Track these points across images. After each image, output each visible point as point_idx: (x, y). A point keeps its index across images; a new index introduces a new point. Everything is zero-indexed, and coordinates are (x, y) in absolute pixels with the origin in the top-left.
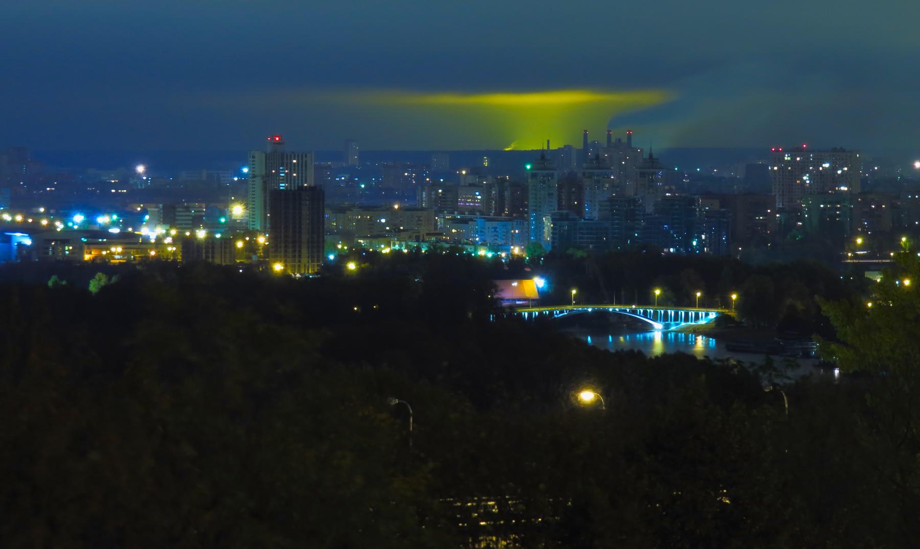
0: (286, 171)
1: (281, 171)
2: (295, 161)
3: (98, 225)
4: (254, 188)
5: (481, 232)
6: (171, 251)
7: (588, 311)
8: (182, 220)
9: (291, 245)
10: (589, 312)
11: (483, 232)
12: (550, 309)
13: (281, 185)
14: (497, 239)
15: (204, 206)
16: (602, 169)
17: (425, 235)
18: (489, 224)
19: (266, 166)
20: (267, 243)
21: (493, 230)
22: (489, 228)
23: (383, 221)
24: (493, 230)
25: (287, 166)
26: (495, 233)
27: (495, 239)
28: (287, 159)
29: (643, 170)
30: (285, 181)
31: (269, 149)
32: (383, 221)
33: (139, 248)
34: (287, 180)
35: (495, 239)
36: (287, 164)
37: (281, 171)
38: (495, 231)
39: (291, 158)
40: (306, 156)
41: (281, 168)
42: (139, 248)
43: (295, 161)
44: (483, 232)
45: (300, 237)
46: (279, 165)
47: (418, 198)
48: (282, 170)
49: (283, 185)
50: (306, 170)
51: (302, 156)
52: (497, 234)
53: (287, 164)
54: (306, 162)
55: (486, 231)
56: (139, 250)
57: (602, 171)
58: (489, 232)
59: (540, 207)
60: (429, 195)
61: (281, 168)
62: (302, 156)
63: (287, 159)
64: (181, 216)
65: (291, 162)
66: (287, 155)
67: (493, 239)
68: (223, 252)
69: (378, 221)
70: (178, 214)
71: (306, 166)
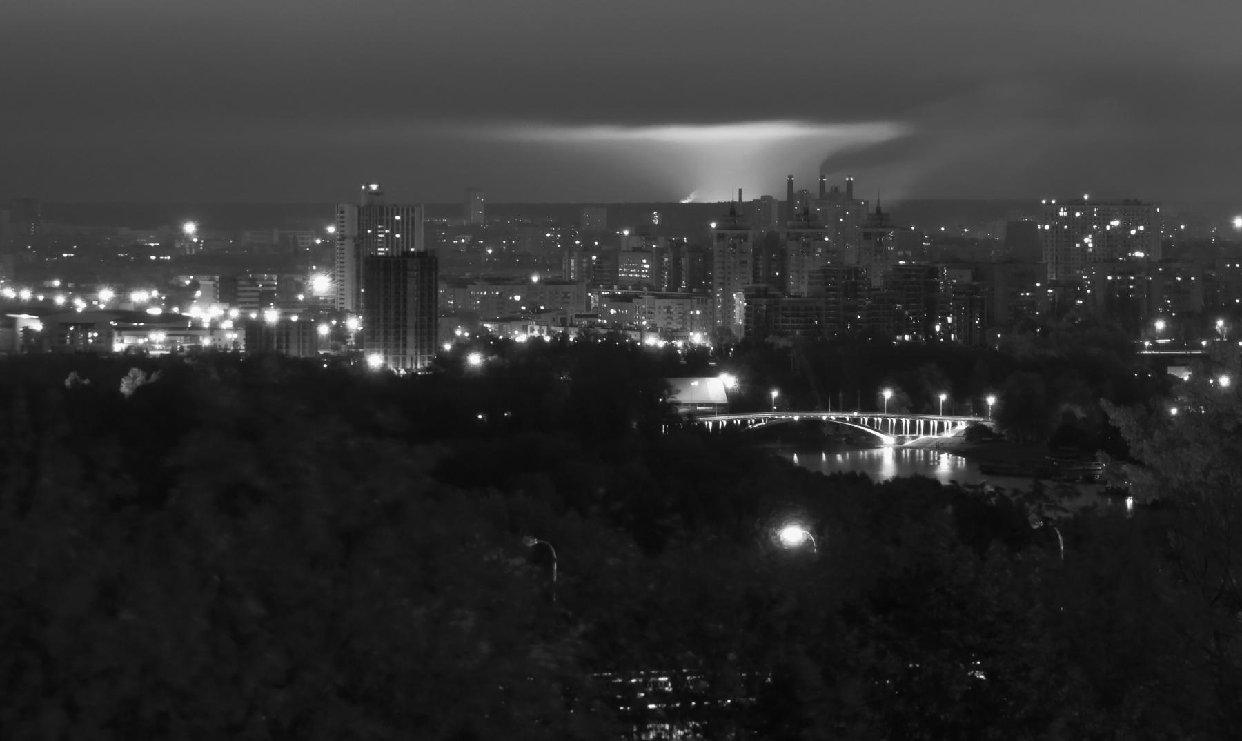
0: (387, 231)
4: (343, 254)
5: (649, 313)
13: (379, 249)
14: (670, 323)
16: (812, 228)
17: (574, 317)
18: (659, 302)
19: (359, 224)
21: (665, 310)
22: (660, 308)
23: (517, 298)
25: (387, 224)
26: (669, 315)
29: (868, 230)
32: (517, 298)
35: (668, 323)
36: (388, 221)
38: (669, 311)
40: (413, 211)
41: (380, 227)
47: (564, 267)
48: (380, 229)
50: (413, 230)
51: (408, 210)
52: (672, 316)
53: (388, 221)
54: (413, 218)
55: (656, 312)
58: (660, 313)
60: (579, 264)
61: (380, 227)
62: (408, 210)
67: (665, 322)
69: (511, 298)
71: (413, 224)
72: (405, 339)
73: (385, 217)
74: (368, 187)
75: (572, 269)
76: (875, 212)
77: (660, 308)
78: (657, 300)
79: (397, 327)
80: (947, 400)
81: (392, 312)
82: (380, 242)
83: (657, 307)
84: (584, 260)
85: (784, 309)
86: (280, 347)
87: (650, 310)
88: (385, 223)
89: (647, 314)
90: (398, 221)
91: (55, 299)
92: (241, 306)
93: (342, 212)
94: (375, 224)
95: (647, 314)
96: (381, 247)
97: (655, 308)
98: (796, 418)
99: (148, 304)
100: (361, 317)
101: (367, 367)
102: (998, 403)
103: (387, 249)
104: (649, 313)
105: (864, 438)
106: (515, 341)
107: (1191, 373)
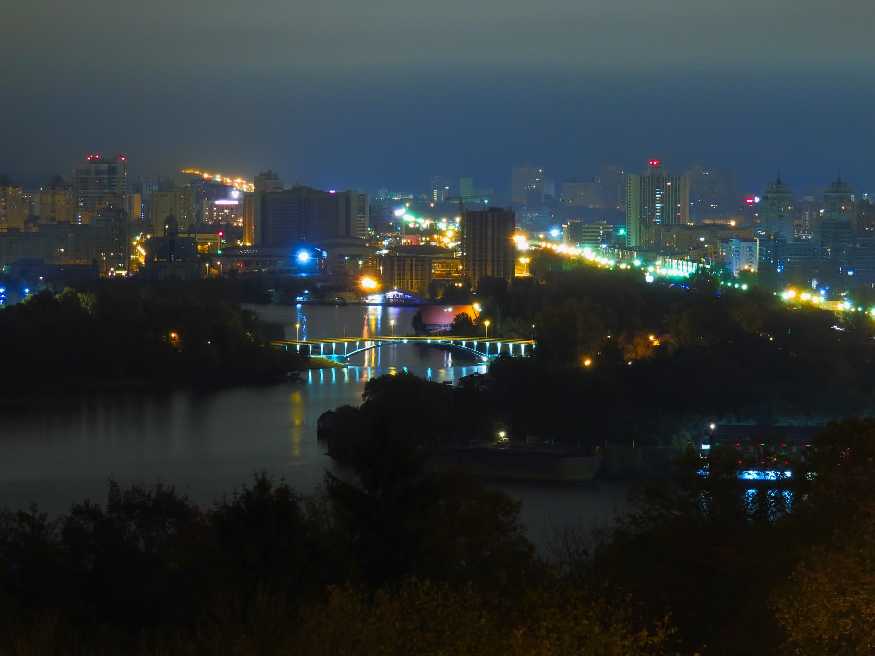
0: (662, 193)
2: (669, 184)
4: (630, 208)
5: (736, 251)
8: (590, 236)
9: (420, 263)
10: (428, 343)
11: (738, 251)
12: (455, 338)
13: (657, 205)
14: (752, 259)
16: (780, 193)
18: (744, 244)
21: (748, 249)
22: (743, 248)
23: (702, 239)
24: (748, 249)
25: (662, 189)
26: (750, 253)
27: (749, 258)
31: (648, 173)
32: (702, 239)
36: (663, 186)
40: (679, 179)
41: (657, 190)
42: (445, 263)
43: (669, 184)
44: (738, 251)
45: (486, 256)
46: (655, 186)
47: (803, 217)
48: (658, 191)
49: (659, 205)
50: (679, 191)
51: (676, 179)
52: (753, 253)
53: (663, 186)
55: (741, 251)
57: (780, 195)
58: (743, 251)
59: (770, 228)
60: (811, 215)
61: (657, 190)
62: (676, 179)
66: (663, 178)
67: (748, 258)
68: (414, 269)
70: (583, 230)
71: (679, 188)
73: (661, 184)
75: (807, 219)
76: (258, 175)
77: (743, 248)
78: (741, 242)
79: (481, 261)
80: (490, 325)
81: (477, 250)
82: (658, 200)
83: (741, 247)
84: (814, 213)
85: (788, 250)
86: (498, 274)
87: (737, 249)
89: (734, 252)
90: (669, 185)
93: (630, 180)
95: (734, 252)
96: (658, 203)
97: (740, 248)
98: (429, 341)
102: (174, 333)
103: (662, 205)
104: (736, 251)
106: (745, 269)
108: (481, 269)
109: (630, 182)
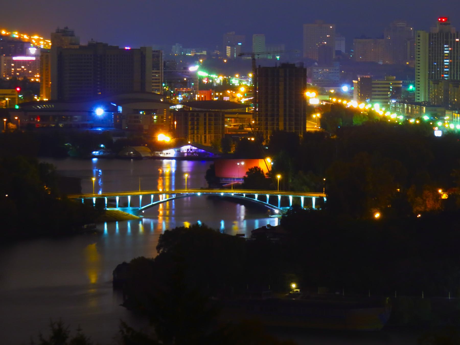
1: (446, 49)
3: (236, 99)
6: (316, 118)
7: (220, 195)
12: (247, 192)
13: (445, 61)
15: (4, 102)
19: (430, 44)
20: (320, 117)
25: (451, 44)
28: (451, 38)
30: (449, 57)
33: (238, 118)
34: (451, 57)
36: (451, 42)
37: (446, 49)
39: (454, 36)
41: (445, 46)
48: (446, 47)
49: (448, 61)
53: (451, 42)
56: (237, 119)
61: (445, 46)
63: (451, 38)
64: (379, 87)
65: (455, 41)
69: (165, 110)
70: (373, 86)
72: (198, 120)
74: (324, 43)
88: (449, 43)
91: (422, 117)
92: (382, 100)
93: (419, 36)
94: (442, 44)
99: (316, 108)
100: (153, 117)
101: (425, 121)
105: (444, 114)
107: (157, 116)
108: (273, 120)
109: (419, 38)
